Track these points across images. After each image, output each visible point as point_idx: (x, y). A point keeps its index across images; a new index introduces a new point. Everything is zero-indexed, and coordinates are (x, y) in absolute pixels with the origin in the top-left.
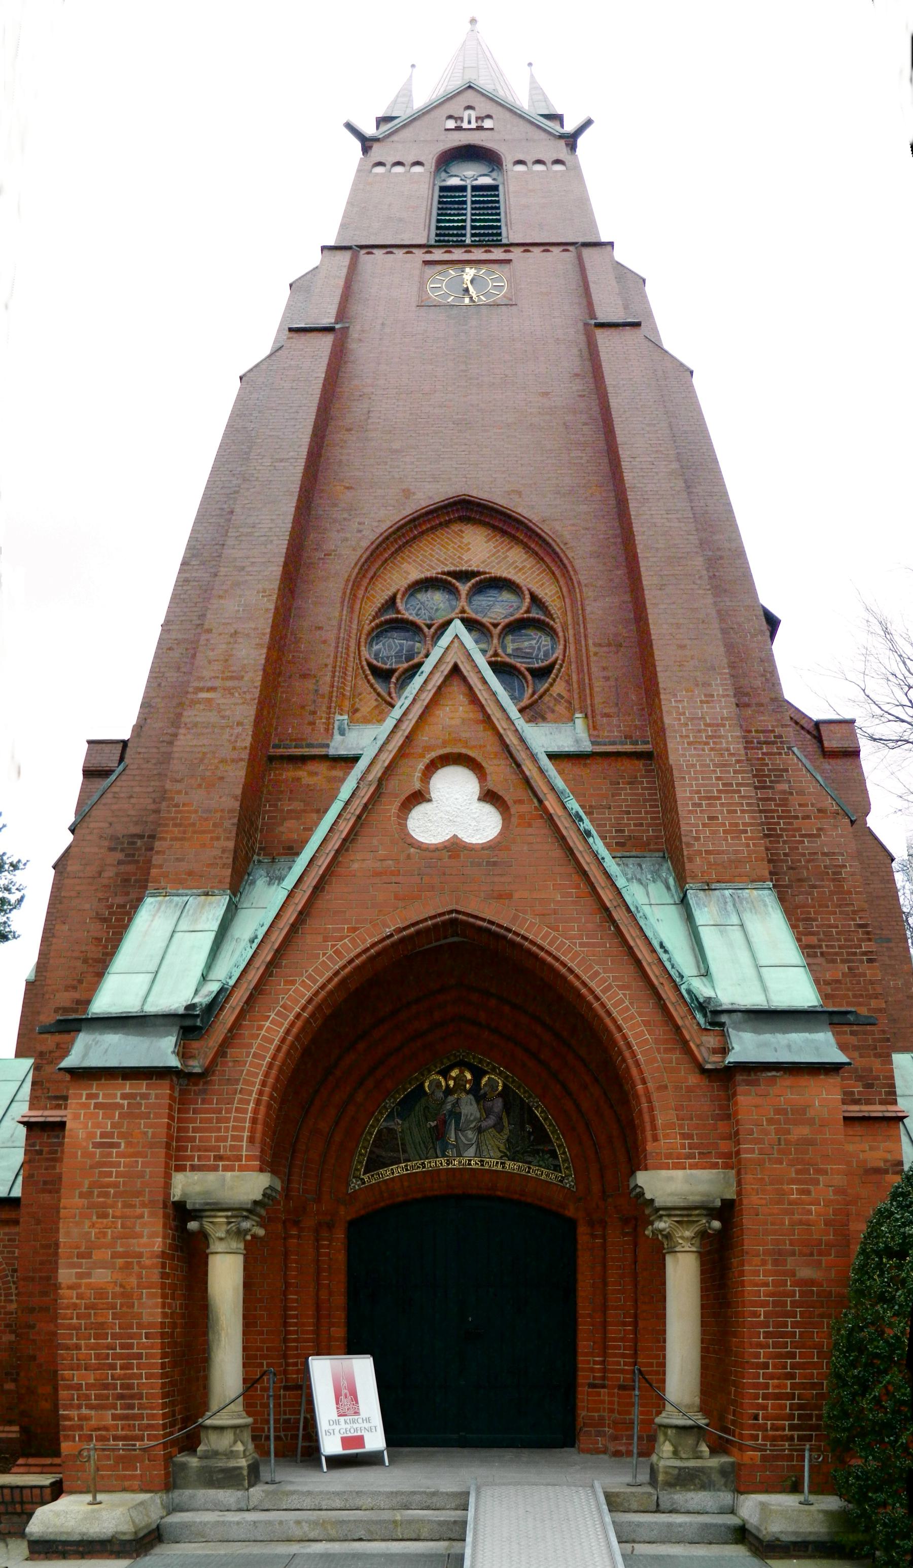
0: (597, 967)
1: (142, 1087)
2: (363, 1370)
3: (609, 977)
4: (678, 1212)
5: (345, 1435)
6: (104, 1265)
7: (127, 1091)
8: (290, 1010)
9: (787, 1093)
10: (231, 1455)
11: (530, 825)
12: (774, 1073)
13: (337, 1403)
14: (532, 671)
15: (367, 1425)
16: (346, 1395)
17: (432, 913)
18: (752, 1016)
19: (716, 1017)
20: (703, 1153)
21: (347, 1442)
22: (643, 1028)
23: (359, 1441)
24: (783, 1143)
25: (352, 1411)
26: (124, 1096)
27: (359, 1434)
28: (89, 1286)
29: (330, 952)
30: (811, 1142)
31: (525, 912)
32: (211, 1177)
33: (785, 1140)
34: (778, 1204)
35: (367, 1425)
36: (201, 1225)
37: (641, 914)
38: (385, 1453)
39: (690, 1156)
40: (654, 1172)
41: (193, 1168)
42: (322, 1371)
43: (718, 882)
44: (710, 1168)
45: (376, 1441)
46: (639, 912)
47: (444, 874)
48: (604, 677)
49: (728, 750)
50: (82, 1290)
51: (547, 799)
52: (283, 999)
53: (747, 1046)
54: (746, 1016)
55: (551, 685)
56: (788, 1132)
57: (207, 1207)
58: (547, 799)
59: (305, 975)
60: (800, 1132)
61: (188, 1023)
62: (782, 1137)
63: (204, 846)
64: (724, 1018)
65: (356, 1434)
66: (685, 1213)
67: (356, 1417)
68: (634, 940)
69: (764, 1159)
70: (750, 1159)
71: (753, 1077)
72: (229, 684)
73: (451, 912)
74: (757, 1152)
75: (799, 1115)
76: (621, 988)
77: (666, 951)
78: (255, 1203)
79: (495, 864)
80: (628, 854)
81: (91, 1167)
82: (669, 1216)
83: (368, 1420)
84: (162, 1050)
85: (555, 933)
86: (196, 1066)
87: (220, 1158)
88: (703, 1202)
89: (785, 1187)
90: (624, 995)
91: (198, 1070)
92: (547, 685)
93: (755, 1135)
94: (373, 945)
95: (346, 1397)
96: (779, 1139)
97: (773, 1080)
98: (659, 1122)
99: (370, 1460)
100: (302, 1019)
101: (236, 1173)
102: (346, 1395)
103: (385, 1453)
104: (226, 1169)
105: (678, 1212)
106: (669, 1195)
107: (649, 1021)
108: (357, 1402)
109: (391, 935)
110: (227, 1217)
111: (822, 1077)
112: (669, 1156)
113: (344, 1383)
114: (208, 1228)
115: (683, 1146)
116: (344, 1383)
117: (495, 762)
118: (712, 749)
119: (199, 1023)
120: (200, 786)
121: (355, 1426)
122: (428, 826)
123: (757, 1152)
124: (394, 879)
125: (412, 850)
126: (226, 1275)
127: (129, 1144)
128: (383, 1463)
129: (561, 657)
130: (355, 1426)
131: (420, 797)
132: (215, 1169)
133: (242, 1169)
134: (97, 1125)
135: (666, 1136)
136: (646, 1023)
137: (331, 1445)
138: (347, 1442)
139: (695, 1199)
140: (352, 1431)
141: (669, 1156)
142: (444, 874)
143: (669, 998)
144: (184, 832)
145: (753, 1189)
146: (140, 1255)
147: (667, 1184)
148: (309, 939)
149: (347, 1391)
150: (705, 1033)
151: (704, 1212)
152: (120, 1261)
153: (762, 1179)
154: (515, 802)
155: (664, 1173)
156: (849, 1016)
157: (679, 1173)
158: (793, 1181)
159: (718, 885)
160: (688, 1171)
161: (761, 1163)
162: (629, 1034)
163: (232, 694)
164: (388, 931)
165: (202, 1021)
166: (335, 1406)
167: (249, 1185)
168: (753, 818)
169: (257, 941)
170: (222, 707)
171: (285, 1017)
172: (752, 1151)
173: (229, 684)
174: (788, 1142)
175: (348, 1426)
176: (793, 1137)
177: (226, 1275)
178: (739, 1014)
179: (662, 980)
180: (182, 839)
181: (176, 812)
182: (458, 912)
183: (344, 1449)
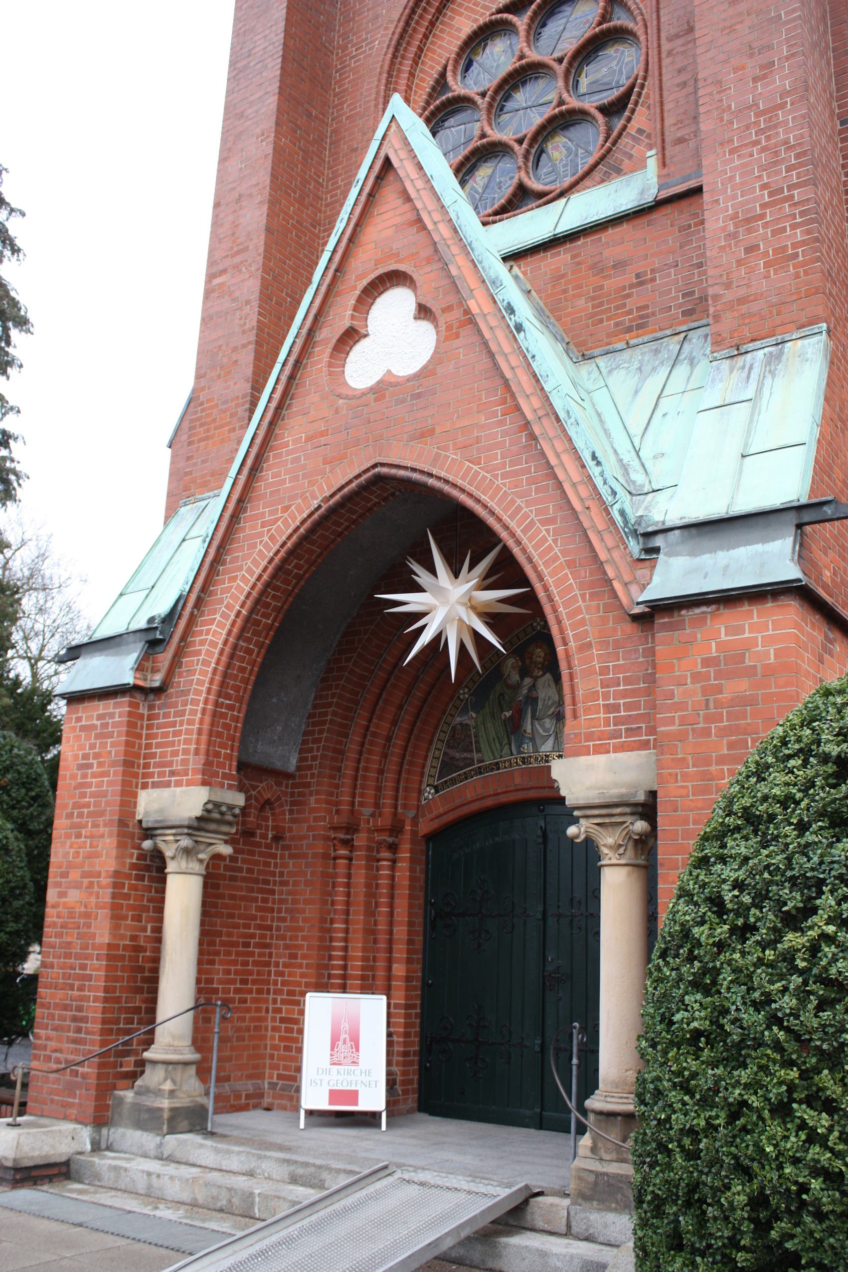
0: (519, 501)
1: (102, 707)
2: (371, 1013)
3: (531, 511)
4: (596, 812)
5: (335, 1088)
6: (77, 886)
7: (101, 712)
8: (561, 594)
9: (720, 631)
10: (158, 1093)
11: (457, 336)
12: (704, 609)
13: (332, 1049)
14: (603, 109)
15: (366, 1079)
16: (345, 1041)
17: (357, 471)
18: (693, 531)
19: (650, 542)
20: (631, 729)
21: (334, 1096)
22: (567, 571)
23: (352, 1096)
24: (712, 705)
25: (349, 1060)
26: (99, 717)
27: (353, 1088)
28: (65, 905)
29: (266, 539)
30: (751, 701)
31: (446, 448)
32: (165, 793)
33: (715, 700)
34: (703, 793)
35: (366, 1079)
36: (155, 843)
37: (573, 420)
38: (384, 1115)
39: (616, 735)
40: (571, 759)
41: (155, 785)
42: (320, 1010)
43: (753, 340)
44: (639, 749)
45: (373, 1099)
46: (569, 417)
47: (369, 422)
48: (678, 85)
49: (786, 142)
50: (60, 909)
51: (473, 297)
52: (227, 599)
53: (677, 574)
54: (686, 532)
55: (629, 120)
56: (719, 690)
57: (156, 825)
58: (473, 297)
59: (245, 568)
60: (741, 686)
61: (151, 637)
62: (712, 698)
63: (223, 441)
64: (658, 541)
65: (349, 1088)
66: (607, 810)
67: (353, 1068)
68: (558, 456)
69: (687, 730)
70: (667, 734)
71: (676, 618)
72: (237, 259)
73: (375, 466)
74: (677, 721)
75: (733, 663)
76: (544, 522)
77: (599, 463)
78: (199, 819)
79: (419, 396)
80: (696, 324)
81: (75, 788)
82: (587, 817)
83: (368, 1073)
84: (119, 669)
85: (475, 468)
86: (156, 680)
87: (173, 773)
88: (622, 795)
89: (713, 768)
90: (548, 531)
91: (157, 684)
92: (623, 122)
93: (676, 700)
94: (303, 522)
95: (346, 1042)
96: (707, 700)
97: (702, 620)
98: (580, 693)
99: (367, 1120)
100: (241, 616)
101: (184, 788)
102: (345, 1041)
103: (384, 1115)
104: (178, 784)
105: (596, 812)
106: (588, 788)
107: (574, 561)
108: (357, 1050)
109: (319, 507)
110: (174, 835)
111: (769, 605)
112: (589, 737)
113: (345, 1026)
114: (162, 846)
115: (607, 722)
116: (345, 1026)
117: (427, 269)
118: (764, 149)
119: (159, 636)
120: (219, 376)
121: (349, 1078)
122: (362, 369)
123: (677, 721)
124: (323, 440)
125: (341, 401)
126: (183, 895)
127: (100, 765)
128: (379, 1126)
129: (641, 73)
130: (349, 1078)
131: (351, 336)
132: (167, 785)
133: (190, 783)
134: (82, 747)
135: (587, 711)
136: (570, 564)
137: (314, 1096)
138: (334, 1096)
139: (614, 793)
140: (345, 1083)
141: (589, 737)
142: (369, 422)
143: (594, 526)
144: (208, 431)
145: (670, 774)
146: (99, 875)
147: (586, 776)
148: (248, 528)
149: (347, 1036)
150: (640, 565)
151: (628, 810)
152: (86, 881)
153: (684, 759)
154: (444, 310)
155: (583, 760)
156: (825, 508)
157: (602, 759)
158: (721, 760)
159: (751, 346)
160: (612, 755)
161: (682, 736)
162: (550, 581)
163: (240, 271)
164: (315, 503)
165: (161, 633)
166: (329, 1052)
167: (186, 800)
168: (808, 232)
169: (208, 540)
170: (232, 289)
171: (566, 605)
172: (671, 721)
173: (237, 259)
174: (718, 704)
175: (340, 1078)
176: (725, 696)
177: (183, 895)
178: (677, 532)
179: (588, 503)
180: (207, 438)
181: (203, 411)
182: (383, 465)
183: (331, 1103)
